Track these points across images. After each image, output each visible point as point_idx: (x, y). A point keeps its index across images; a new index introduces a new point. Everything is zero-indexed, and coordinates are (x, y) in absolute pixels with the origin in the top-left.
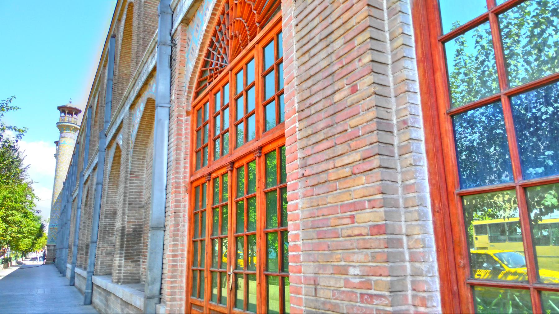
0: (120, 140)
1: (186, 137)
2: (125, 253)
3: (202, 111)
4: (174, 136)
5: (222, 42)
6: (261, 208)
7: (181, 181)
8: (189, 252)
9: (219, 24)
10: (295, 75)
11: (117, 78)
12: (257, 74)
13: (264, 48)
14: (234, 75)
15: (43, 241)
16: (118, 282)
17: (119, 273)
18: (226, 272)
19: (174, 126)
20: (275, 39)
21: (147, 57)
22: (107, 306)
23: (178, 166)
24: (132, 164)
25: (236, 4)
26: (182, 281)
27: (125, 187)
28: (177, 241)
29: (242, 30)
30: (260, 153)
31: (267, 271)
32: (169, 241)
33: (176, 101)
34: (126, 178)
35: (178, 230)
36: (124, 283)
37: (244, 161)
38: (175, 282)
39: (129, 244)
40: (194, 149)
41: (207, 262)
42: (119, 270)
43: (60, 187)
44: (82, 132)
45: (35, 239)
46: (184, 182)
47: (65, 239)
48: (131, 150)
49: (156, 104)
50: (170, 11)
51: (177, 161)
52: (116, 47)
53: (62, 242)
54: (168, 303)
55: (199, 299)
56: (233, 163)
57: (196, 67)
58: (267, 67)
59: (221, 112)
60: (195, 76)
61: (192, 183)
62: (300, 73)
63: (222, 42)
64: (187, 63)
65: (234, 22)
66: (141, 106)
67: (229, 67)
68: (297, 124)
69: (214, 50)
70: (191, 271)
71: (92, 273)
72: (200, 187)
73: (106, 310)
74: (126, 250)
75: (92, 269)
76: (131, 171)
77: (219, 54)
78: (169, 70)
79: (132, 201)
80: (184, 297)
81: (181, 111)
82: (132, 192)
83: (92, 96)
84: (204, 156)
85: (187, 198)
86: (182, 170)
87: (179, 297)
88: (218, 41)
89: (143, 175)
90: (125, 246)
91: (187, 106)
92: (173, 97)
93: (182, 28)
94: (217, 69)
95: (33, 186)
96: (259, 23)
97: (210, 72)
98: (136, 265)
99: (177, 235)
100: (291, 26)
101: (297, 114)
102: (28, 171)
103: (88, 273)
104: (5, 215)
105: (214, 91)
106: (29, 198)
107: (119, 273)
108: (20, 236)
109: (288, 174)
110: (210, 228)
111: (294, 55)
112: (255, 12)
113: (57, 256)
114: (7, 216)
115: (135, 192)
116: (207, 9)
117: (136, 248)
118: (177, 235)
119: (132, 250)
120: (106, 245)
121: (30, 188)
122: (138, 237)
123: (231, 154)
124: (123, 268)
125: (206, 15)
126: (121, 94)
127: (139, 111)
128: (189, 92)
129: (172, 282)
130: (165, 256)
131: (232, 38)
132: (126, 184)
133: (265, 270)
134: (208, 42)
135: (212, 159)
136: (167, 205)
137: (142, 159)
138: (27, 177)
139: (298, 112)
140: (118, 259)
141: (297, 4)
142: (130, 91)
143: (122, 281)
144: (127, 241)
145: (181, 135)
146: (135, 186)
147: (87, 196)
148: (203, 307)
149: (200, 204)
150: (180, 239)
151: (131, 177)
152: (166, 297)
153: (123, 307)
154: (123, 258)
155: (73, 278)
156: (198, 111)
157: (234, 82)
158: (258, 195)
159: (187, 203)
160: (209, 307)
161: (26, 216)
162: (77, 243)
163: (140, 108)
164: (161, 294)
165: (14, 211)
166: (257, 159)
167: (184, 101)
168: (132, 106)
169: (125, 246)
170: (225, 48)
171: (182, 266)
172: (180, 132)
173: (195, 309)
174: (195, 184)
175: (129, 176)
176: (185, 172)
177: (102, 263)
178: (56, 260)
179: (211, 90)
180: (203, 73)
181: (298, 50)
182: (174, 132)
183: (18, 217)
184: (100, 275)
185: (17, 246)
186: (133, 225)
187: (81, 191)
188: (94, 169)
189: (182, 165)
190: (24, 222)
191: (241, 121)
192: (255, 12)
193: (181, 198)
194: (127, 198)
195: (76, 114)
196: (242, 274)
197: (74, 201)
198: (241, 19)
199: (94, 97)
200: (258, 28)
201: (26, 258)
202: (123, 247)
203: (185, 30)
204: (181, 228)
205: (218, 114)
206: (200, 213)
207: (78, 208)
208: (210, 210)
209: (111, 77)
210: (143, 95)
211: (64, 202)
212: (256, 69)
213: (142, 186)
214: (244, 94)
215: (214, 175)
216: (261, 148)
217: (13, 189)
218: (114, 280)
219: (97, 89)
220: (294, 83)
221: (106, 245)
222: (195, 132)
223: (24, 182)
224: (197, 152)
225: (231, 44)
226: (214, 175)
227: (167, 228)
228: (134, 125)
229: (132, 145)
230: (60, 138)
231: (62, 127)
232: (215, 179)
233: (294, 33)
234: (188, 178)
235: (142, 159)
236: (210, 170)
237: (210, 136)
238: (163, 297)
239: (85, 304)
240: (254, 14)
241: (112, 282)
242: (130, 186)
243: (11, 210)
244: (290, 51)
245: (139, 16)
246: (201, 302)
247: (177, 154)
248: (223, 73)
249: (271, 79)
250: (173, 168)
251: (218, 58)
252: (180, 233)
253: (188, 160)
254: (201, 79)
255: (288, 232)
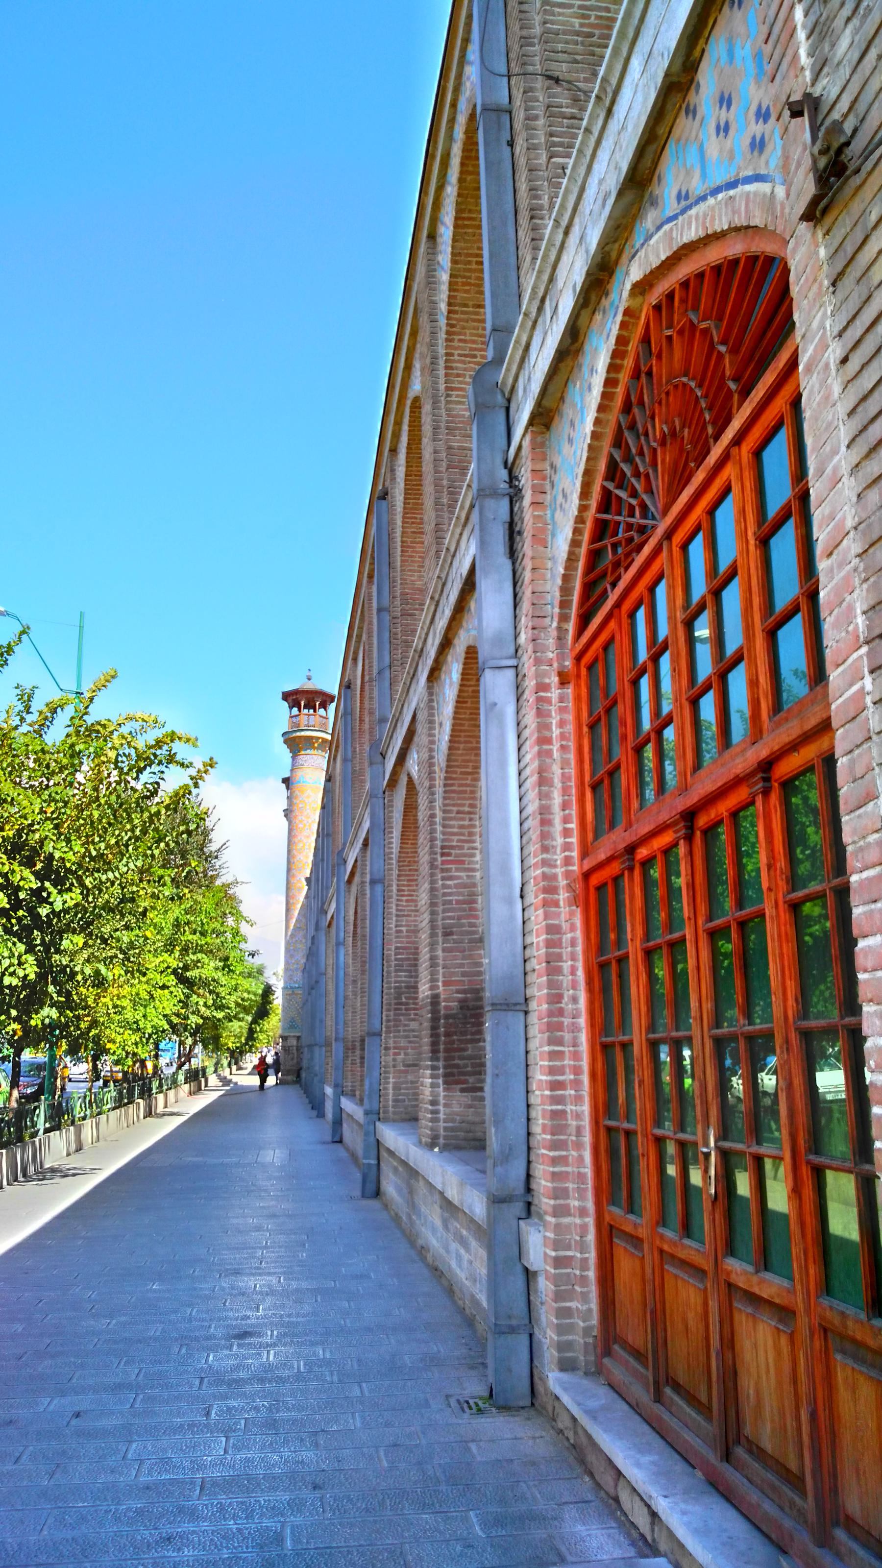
0: (413, 765)
1: (562, 746)
2: (445, 1067)
3: (599, 667)
4: (531, 747)
5: (637, 459)
6: (781, 955)
7: (559, 871)
8: (593, 1075)
9: (627, 408)
10: (850, 523)
11: (398, 602)
12: (743, 535)
13: (757, 453)
14: (676, 550)
15: (274, 1023)
16: (431, 1146)
17: (433, 1120)
18: (695, 1144)
19: (530, 719)
20: (788, 420)
21: (457, 536)
22: (412, 1205)
23: (546, 829)
24: (444, 826)
25: (669, 338)
26: (581, 1159)
27: (433, 890)
28: (560, 1042)
29: (689, 412)
30: (766, 780)
31: (817, 1152)
32: (539, 1045)
33: (530, 650)
34: (432, 866)
35: (561, 1012)
36: (445, 1148)
37: (723, 808)
38: (563, 1161)
39: (453, 1042)
40: (587, 778)
41: (643, 1109)
42: (432, 1112)
43: (302, 891)
44: (336, 751)
45: (255, 1021)
46: (567, 874)
47: (318, 1022)
48: (439, 790)
49: (480, 660)
50: (500, 400)
51: (544, 812)
52: (391, 523)
53: (312, 1028)
54: (549, 1218)
55: (631, 1217)
56: (689, 816)
57: (575, 543)
58: (773, 508)
59: (650, 666)
60: (576, 569)
61: (586, 876)
62: (864, 516)
63: (637, 459)
64: (553, 535)
65: (667, 394)
66: (454, 671)
67: (662, 527)
68: (868, 682)
69: (620, 486)
70: (602, 1132)
71: (376, 1115)
72: (610, 888)
73: (409, 1216)
74: (446, 1059)
75: (375, 1106)
76: (442, 847)
77: (634, 494)
78: (508, 563)
79: (452, 926)
80: (590, 1205)
81: (546, 674)
82: (450, 902)
83: (350, 657)
84: (612, 797)
85: (578, 921)
86: (559, 840)
87: (576, 1203)
88: (628, 458)
89: (473, 855)
90: (442, 1047)
91: (561, 657)
92: (523, 638)
93: (533, 441)
94: (630, 540)
95: (238, 891)
96: (736, 379)
97: (614, 551)
98: (474, 1099)
99: (559, 1027)
100: (827, 365)
101: (864, 650)
102: (225, 856)
103: (367, 1113)
104: (181, 965)
105: (626, 606)
106: (230, 921)
107: (433, 1120)
108: (220, 1015)
109: (849, 849)
110: (644, 1009)
111: (844, 460)
112: (723, 349)
113: (305, 1064)
114: (186, 968)
115: (458, 902)
116: (592, 370)
117: (469, 1052)
118: (559, 1027)
119: (460, 1058)
120: (403, 1043)
121: (232, 898)
122: (473, 1025)
123: (684, 788)
124: (441, 1108)
125: (590, 389)
126: (407, 644)
127: (451, 684)
128: (564, 618)
129: (554, 1161)
130: (534, 1086)
131: (663, 443)
132: (433, 882)
133: (809, 1150)
134: (602, 466)
135: (635, 804)
136: (528, 940)
137: (470, 813)
138: (224, 871)
139: (867, 643)
140: (428, 1084)
141: (840, 295)
142: (427, 634)
143: (442, 1141)
144: (447, 1034)
145: (549, 741)
146: (456, 886)
147: (356, 913)
148: (641, 1240)
149: (612, 936)
150: (568, 1037)
151: (443, 862)
152: (545, 1203)
153: (446, 1215)
154: (440, 1081)
155: (338, 1123)
156: (590, 667)
157: (678, 572)
158: (769, 912)
159: (579, 934)
160: (658, 1243)
161: (227, 966)
162: (341, 1036)
163: (451, 678)
164: (529, 1190)
165: (199, 955)
166: (759, 800)
167: (550, 647)
168: (434, 674)
169: (442, 1047)
170: (647, 476)
171: (578, 1116)
172: (547, 734)
173: (623, 1244)
174: (595, 880)
175: (439, 859)
176: (567, 847)
177: (396, 1088)
178: (303, 1075)
179: (618, 605)
180: (594, 556)
181: (853, 440)
182: (532, 734)
183: (209, 968)
184: (394, 1121)
185: (216, 1039)
186: (458, 992)
187: (342, 901)
188: (366, 844)
189: (558, 826)
190: (223, 980)
191: (706, 688)
192: (723, 349)
193: (562, 921)
194: (440, 917)
195: (324, 706)
196: (742, 1153)
197: (329, 925)
198: (685, 379)
199: (355, 660)
200: (736, 397)
201: (240, 1068)
202: (438, 1052)
203: (542, 445)
204: (567, 1005)
205: (642, 672)
206: (614, 964)
207: (338, 944)
208: (640, 955)
209: (386, 602)
210: (456, 641)
211: (314, 929)
212: (738, 522)
213: (474, 885)
214: (709, 604)
215: (643, 852)
216: (767, 766)
217: (196, 902)
218: (424, 1140)
219: (359, 637)
220: (849, 548)
221: (403, 1043)
222: (585, 729)
223: (218, 883)
224: (594, 787)
225: (663, 461)
226: (643, 852)
227: (533, 1005)
228: (441, 724)
229: (440, 776)
230: (292, 770)
231: (295, 744)
232: (647, 863)
233: (837, 389)
234: (576, 861)
235: (470, 813)
236: (629, 837)
237: (624, 737)
238: (536, 1201)
239: (364, 1196)
240: (720, 356)
241: (420, 1142)
242: (444, 886)
243: (194, 953)
244: (827, 448)
245: (436, 428)
246: (635, 1225)
247: (541, 796)
248: (647, 550)
249: (784, 545)
250: (534, 835)
251: (632, 508)
252: (567, 1021)
253: (574, 812)
254: (592, 575)
255: (865, 1039)
